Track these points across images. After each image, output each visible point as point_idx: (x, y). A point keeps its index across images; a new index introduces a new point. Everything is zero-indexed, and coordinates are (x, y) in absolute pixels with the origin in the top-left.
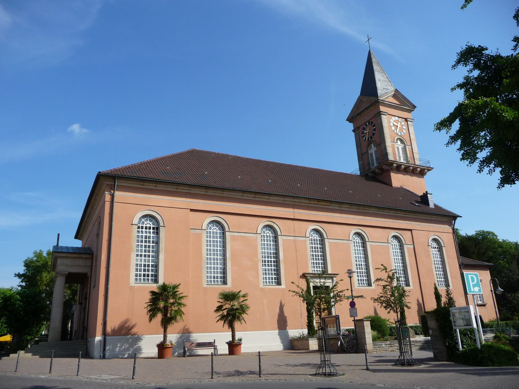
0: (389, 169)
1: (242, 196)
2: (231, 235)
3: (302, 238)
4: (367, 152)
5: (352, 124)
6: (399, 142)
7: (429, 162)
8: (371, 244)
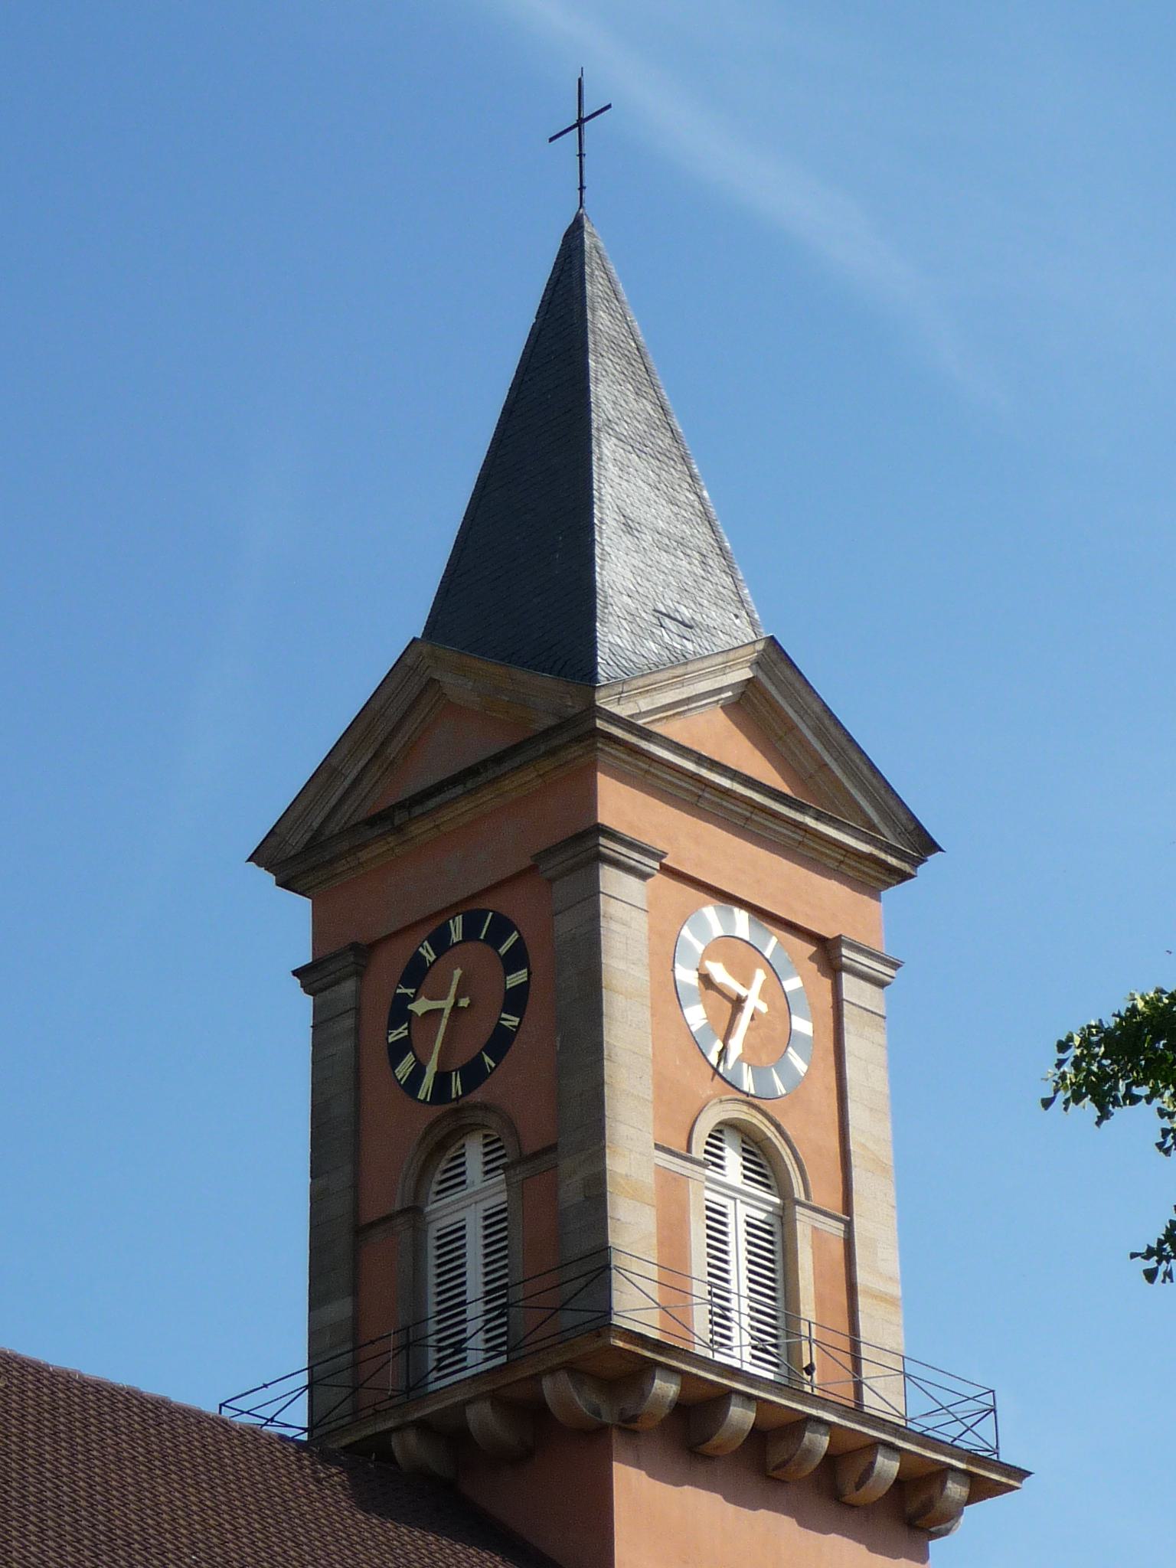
0: (607, 1418)
4: (414, 1212)
6: (733, 1159)
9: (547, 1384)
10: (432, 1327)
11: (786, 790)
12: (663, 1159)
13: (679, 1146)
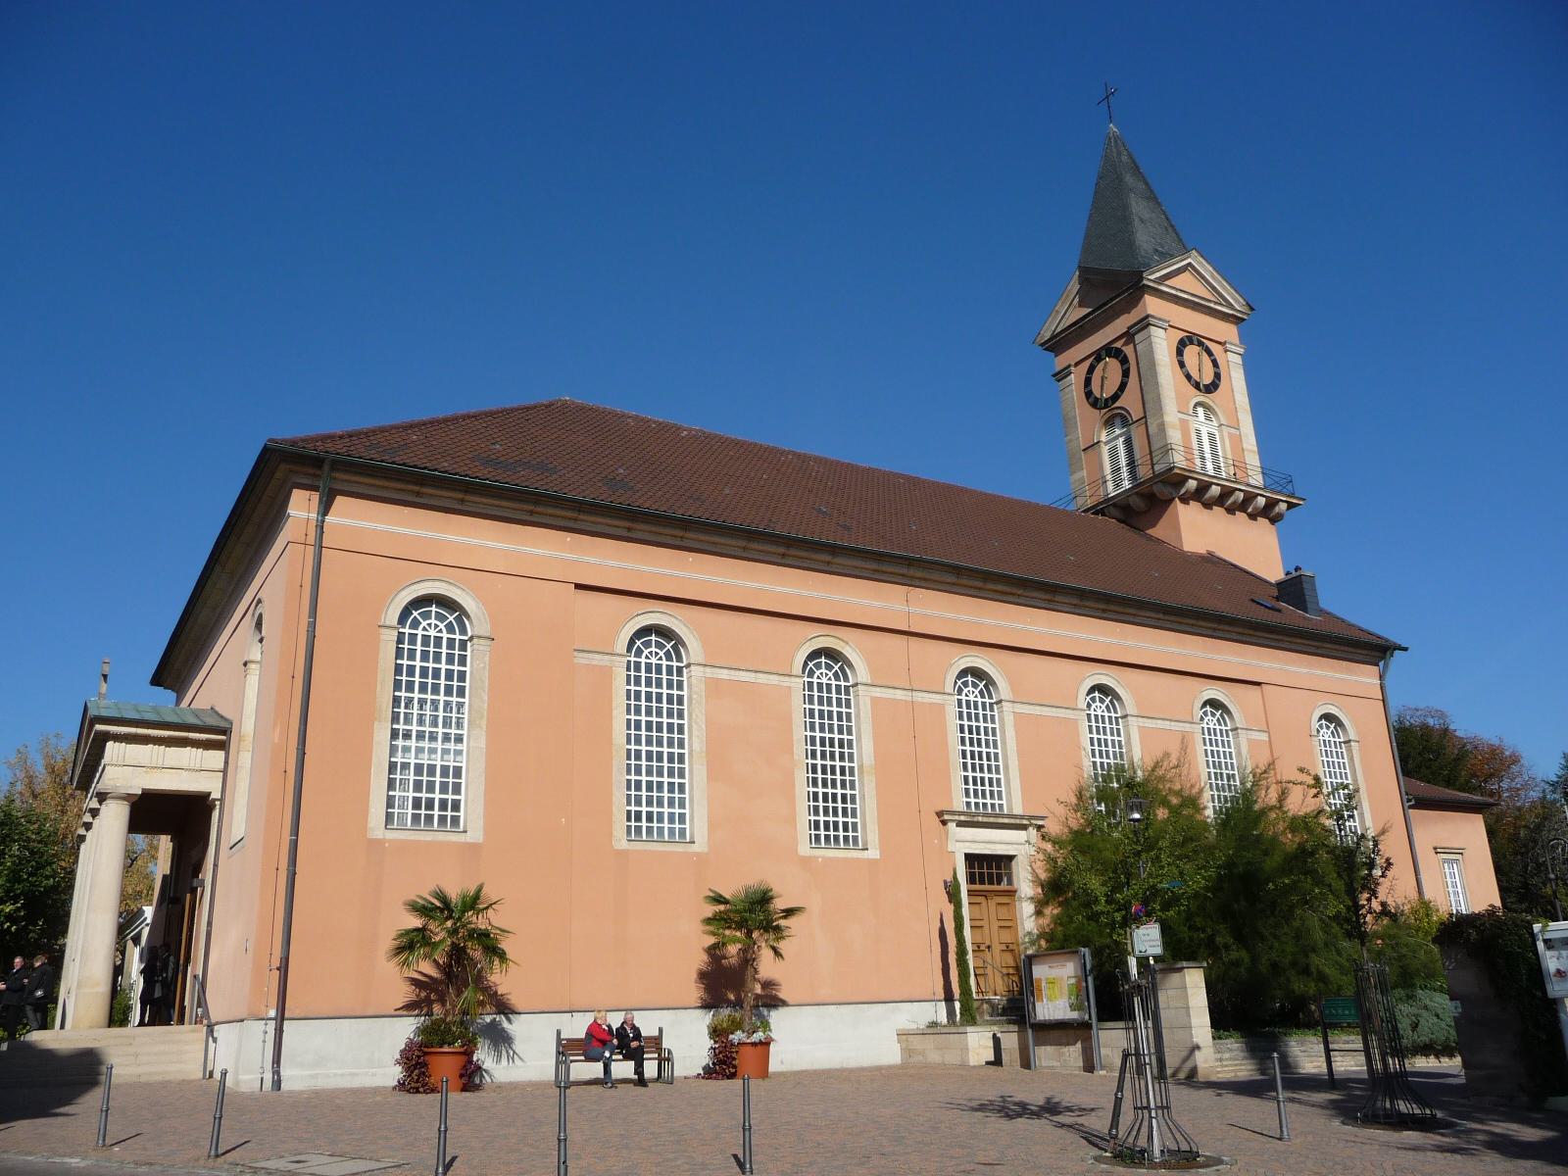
1: (744, 548)
3: (930, 695)
6: (1200, 410)
8: (1141, 725)
11: (1090, 310)
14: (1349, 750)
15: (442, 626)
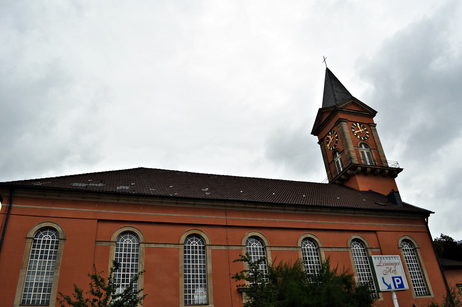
0: (355, 173)
2: (146, 246)
3: (236, 247)
4: (333, 161)
5: (317, 136)
6: (363, 146)
7: (398, 164)
8: (325, 250)
9: (348, 172)
10: (337, 169)
11: (360, 110)
12: (355, 148)
13: (356, 146)
14: (416, 251)
15: (194, 242)
